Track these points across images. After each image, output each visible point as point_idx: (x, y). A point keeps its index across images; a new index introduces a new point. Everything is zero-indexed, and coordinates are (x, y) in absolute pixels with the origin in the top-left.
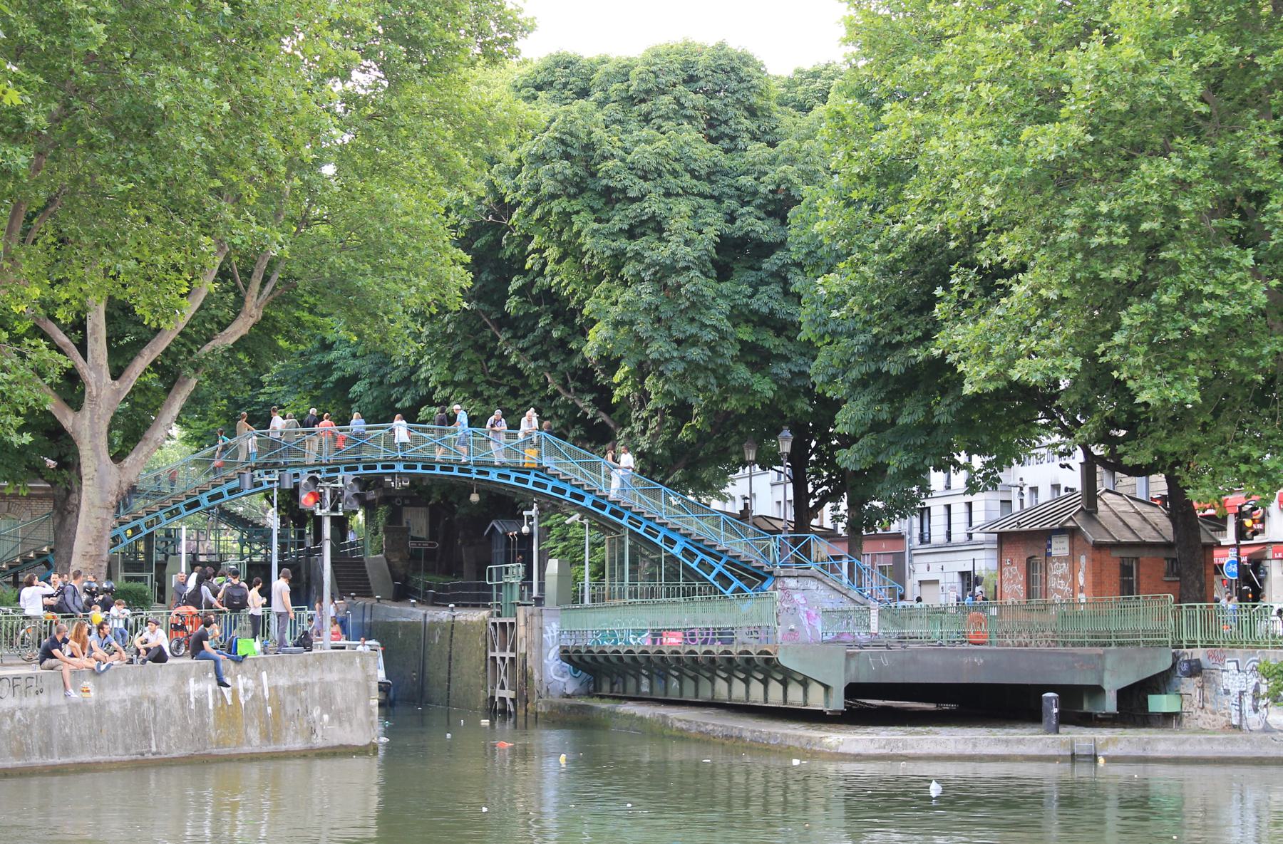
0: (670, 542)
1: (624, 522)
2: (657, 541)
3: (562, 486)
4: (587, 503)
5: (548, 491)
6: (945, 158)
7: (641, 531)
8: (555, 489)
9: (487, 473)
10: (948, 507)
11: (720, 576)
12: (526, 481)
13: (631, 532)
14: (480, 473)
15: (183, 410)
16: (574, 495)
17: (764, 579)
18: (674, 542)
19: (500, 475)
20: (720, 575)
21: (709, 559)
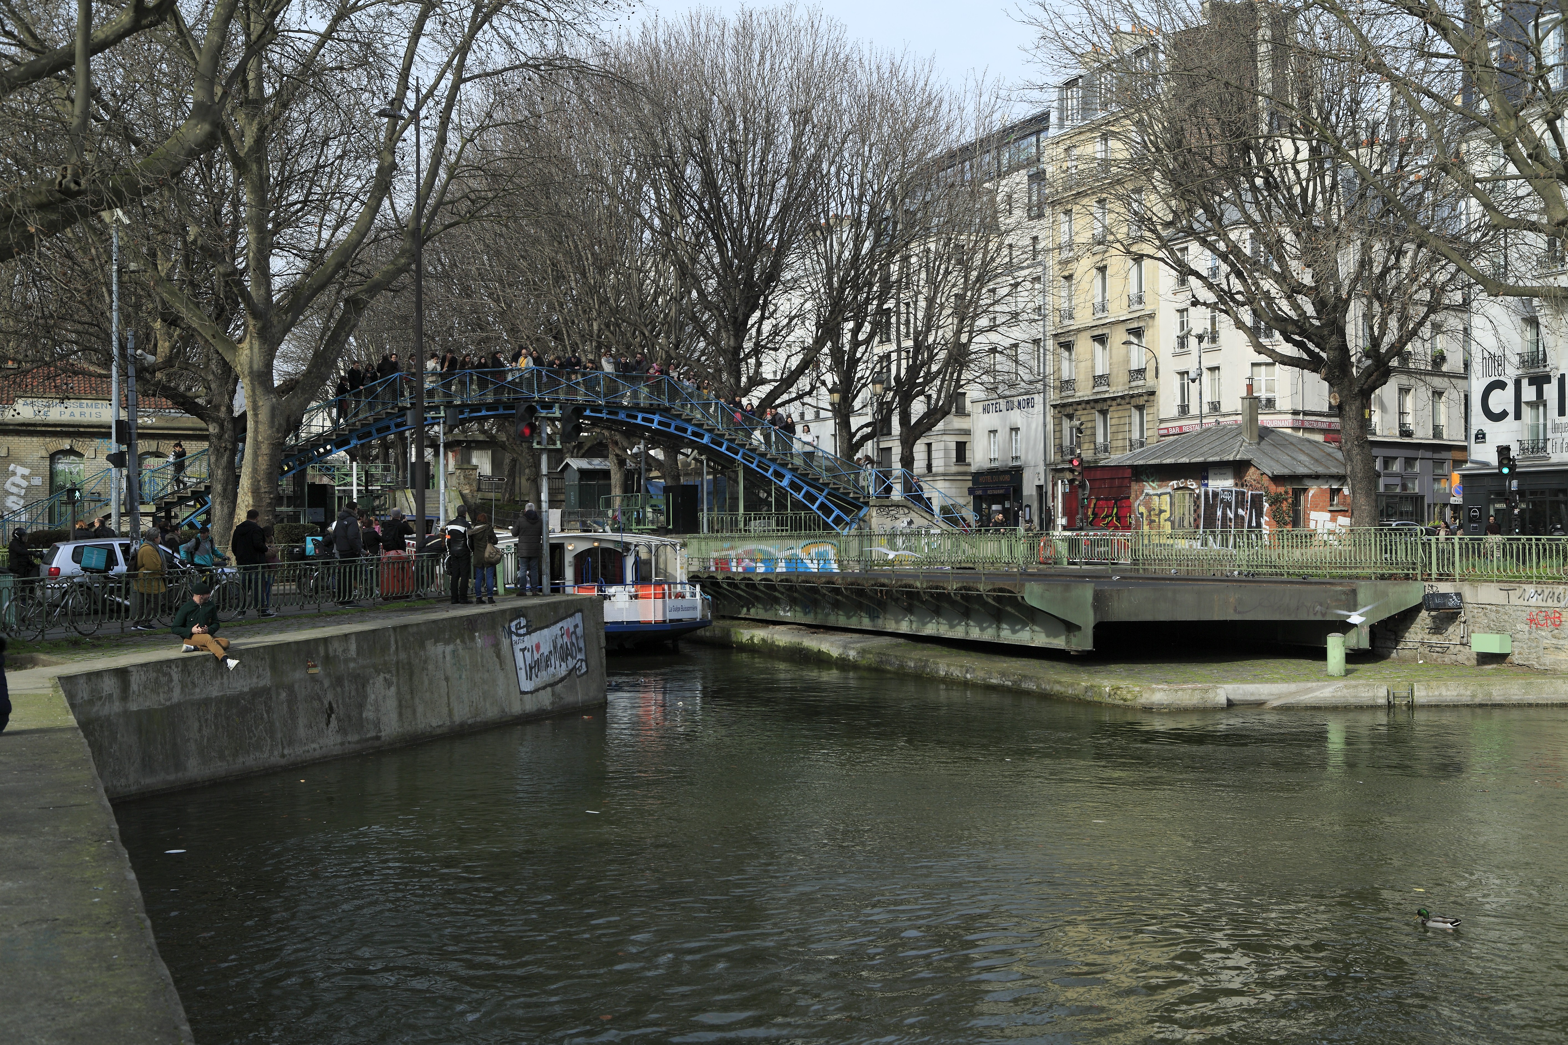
0: (779, 475)
1: (738, 457)
2: (768, 475)
3: (686, 425)
4: (706, 440)
5: (672, 430)
6: (1053, 396)
7: (754, 466)
8: (677, 428)
9: (636, 417)
10: (929, 445)
11: (822, 506)
12: (652, 421)
13: (745, 466)
14: (610, 413)
15: (358, 634)
16: (694, 434)
17: (860, 508)
18: (783, 476)
19: (628, 416)
20: (822, 506)
21: (812, 490)
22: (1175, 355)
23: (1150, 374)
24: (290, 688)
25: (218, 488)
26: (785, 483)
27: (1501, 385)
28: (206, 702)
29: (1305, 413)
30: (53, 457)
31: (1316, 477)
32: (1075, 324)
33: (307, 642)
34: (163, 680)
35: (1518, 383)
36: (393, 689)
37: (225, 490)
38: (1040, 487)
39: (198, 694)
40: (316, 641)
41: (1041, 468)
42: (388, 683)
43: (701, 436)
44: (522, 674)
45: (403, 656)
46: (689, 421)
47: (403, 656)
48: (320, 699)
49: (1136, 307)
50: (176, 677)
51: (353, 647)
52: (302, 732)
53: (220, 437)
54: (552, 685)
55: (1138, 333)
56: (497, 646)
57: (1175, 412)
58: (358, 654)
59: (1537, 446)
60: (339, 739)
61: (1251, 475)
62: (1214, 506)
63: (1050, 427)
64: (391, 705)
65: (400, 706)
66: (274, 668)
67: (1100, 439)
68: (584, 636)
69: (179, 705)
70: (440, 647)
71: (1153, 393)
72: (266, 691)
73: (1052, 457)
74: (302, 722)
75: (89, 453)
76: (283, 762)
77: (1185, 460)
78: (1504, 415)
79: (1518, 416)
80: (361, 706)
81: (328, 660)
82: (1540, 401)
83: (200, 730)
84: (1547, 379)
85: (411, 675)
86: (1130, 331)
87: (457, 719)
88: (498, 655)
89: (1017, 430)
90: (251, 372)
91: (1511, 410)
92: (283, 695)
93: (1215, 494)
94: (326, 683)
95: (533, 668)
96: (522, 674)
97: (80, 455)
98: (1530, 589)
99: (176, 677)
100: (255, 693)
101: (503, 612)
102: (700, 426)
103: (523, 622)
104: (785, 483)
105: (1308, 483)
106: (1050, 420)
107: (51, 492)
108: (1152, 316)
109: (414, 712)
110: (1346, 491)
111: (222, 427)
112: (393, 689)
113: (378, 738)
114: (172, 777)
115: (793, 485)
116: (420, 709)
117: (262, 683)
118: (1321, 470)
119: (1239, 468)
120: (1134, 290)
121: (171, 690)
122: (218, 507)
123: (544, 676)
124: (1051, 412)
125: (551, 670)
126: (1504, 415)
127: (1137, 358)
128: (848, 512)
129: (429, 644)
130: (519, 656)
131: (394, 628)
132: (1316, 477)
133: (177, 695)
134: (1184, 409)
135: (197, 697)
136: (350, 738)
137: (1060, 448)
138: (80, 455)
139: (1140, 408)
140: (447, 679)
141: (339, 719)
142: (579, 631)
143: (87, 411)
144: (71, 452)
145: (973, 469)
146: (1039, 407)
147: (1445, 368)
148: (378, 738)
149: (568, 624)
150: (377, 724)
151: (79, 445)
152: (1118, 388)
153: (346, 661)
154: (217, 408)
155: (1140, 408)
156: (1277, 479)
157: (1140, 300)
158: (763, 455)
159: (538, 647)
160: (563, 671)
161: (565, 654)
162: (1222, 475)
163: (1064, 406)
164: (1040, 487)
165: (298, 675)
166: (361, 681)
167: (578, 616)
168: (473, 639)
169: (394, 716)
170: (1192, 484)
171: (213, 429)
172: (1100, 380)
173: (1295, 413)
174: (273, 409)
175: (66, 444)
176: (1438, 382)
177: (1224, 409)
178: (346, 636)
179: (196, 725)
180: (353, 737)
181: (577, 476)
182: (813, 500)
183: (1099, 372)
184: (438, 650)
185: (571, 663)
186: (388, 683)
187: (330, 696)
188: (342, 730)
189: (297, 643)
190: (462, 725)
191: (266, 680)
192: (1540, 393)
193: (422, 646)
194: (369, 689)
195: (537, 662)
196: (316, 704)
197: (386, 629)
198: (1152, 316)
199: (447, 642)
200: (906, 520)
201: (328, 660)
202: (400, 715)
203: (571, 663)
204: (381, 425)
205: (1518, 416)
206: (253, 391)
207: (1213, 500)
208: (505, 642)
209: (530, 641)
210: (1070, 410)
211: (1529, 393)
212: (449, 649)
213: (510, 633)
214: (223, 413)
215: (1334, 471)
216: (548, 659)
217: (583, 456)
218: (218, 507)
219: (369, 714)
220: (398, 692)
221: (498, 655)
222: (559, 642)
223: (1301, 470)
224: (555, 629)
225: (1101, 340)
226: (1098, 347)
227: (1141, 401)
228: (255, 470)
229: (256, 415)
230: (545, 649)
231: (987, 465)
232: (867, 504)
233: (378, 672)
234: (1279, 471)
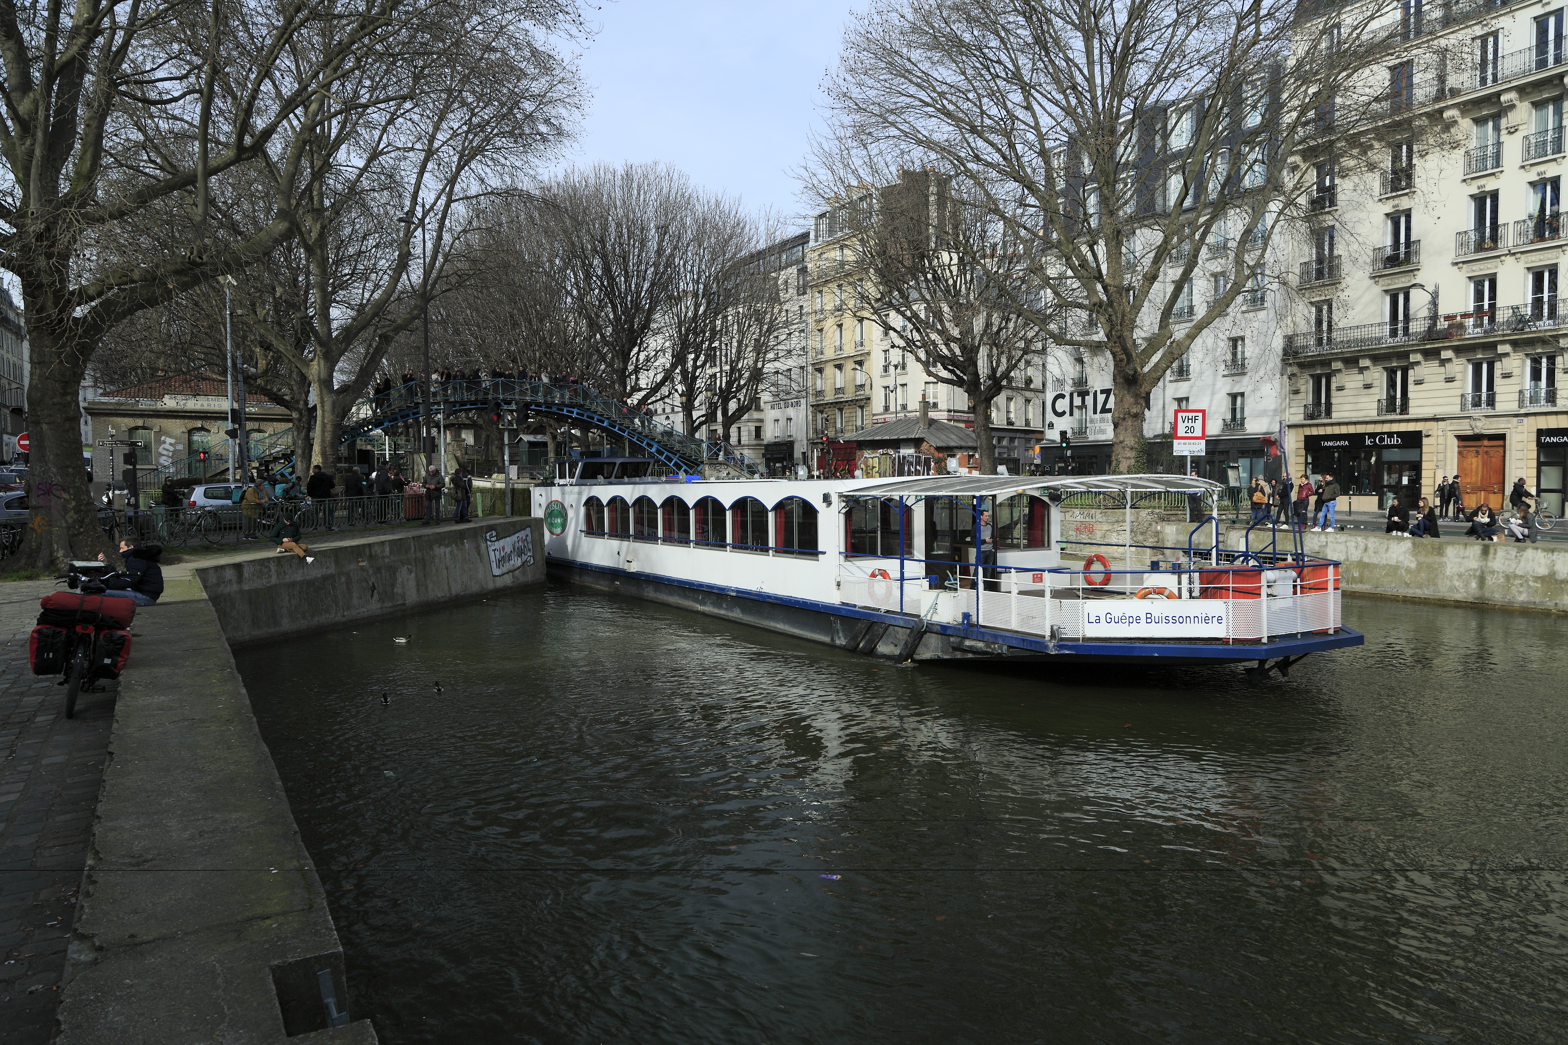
5: (585, 418)
6: (812, 400)
11: (676, 464)
15: (390, 541)
16: (598, 420)
20: (676, 464)
22: (882, 377)
23: (867, 387)
24: (348, 575)
25: (299, 451)
26: (653, 450)
27: (1062, 396)
28: (293, 584)
29: (955, 411)
30: (191, 432)
31: (960, 448)
32: (824, 358)
33: (358, 546)
34: (265, 570)
35: (1071, 395)
36: (413, 575)
37: (303, 453)
38: (804, 453)
39: (288, 579)
40: (364, 546)
41: (805, 442)
42: (410, 571)
43: (603, 422)
44: (494, 565)
45: (419, 554)
46: (595, 412)
47: (419, 554)
48: (367, 581)
49: (859, 348)
50: (273, 568)
51: (387, 549)
52: (355, 601)
53: (300, 420)
54: (513, 571)
55: (860, 363)
56: (478, 548)
57: (881, 410)
58: (391, 553)
59: (1081, 431)
60: (379, 605)
61: (924, 446)
62: (903, 465)
63: (810, 418)
64: (412, 583)
65: (418, 585)
66: (337, 562)
67: (839, 425)
68: (532, 542)
69: (275, 586)
70: (442, 549)
71: (869, 399)
72: (332, 576)
73: (811, 435)
74: (355, 595)
75: (214, 430)
76: (344, 619)
77: (887, 437)
78: (1064, 413)
79: (1071, 414)
80: (393, 585)
81: (371, 557)
82: (1083, 406)
83: (290, 601)
84: (1087, 393)
85: (424, 566)
86: (856, 362)
87: (454, 592)
88: (479, 554)
89: (790, 419)
90: (319, 380)
91: (1068, 411)
92: (343, 579)
93: (904, 457)
94: (371, 572)
95: (501, 561)
96: (494, 565)
97: (208, 431)
98: (1077, 512)
99: (273, 568)
100: (325, 578)
101: (482, 527)
102: (602, 415)
103: (494, 533)
104: (653, 450)
105: (956, 451)
106: (809, 413)
107: (189, 454)
108: (868, 354)
109: (427, 589)
110: (977, 456)
111: (301, 414)
112: (413, 575)
113: (404, 604)
114: (272, 630)
115: (658, 451)
116: (430, 586)
117: (329, 572)
118: (963, 444)
119: (917, 442)
120: (858, 339)
121: (270, 577)
122: (299, 463)
123: (507, 567)
124: (810, 409)
125: (512, 562)
126: (1064, 413)
127: (860, 378)
128: (691, 467)
129: (435, 547)
130: (492, 554)
131: (413, 538)
132: (960, 448)
133: (274, 580)
134: (887, 408)
135: (287, 581)
136: (386, 605)
137: (816, 431)
138: (208, 431)
139: (862, 407)
140: (447, 568)
141: (379, 594)
142: (529, 539)
143: (212, 403)
144: (202, 429)
145: (765, 442)
146: (803, 406)
147: (1032, 386)
148: (404, 604)
149: (522, 534)
150: (403, 596)
151: (207, 425)
152: (849, 396)
153: (383, 558)
154: (298, 402)
155: (862, 407)
156: (939, 449)
157: (862, 344)
158: (640, 433)
159: (503, 548)
160: (519, 562)
161: (520, 553)
162: (909, 447)
163: (818, 405)
164: (804, 453)
165: (352, 566)
166: (393, 570)
167: (528, 530)
168: (463, 544)
169: (414, 591)
170: (891, 452)
171: (295, 415)
172: (838, 391)
173: (949, 411)
174: (334, 404)
175: (199, 424)
176: (1028, 394)
177: (909, 409)
178: (383, 543)
179: (287, 598)
180: (388, 604)
181: (527, 445)
182: (670, 460)
183: (838, 386)
184: (441, 551)
185: (524, 558)
186: (410, 571)
187: (373, 579)
188: (381, 600)
189: (351, 547)
190: (457, 596)
191: (332, 570)
192: (1083, 401)
193: (431, 548)
194: (397, 575)
195: (503, 558)
196: (364, 584)
197: (408, 538)
198: (868, 354)
199: (447, 546)
200: (725, 472)
201: (371, 557)
202: (418, 590)
203: (524, 558)
204: (403, 413)
205: (1071, 414)
206: (321, 391)
207: (903, 461)
208: (483, 546)
209: (498, 545)
210: (821, 408)
211: (1077, 401)
212: (448, 550)
213: (486, 540)
214: (301, 405)
215: (970, 444)
216: (510, 556)
217: (531, 434)
218: (299, 463)
219: (398, 590)
220: (417, 577)
221: (479, 554)
222: (517, 545)
223: (952, 444)
224: (514, 538)
225: (839, 367)
226: (838, 371)
227: (862, 403)
228: (323, 441)
229: (323, 406)
230: (508, 550)
231: (773, 440)
232: (702, 462)
233: (403, 564)
234: (940, 444)
